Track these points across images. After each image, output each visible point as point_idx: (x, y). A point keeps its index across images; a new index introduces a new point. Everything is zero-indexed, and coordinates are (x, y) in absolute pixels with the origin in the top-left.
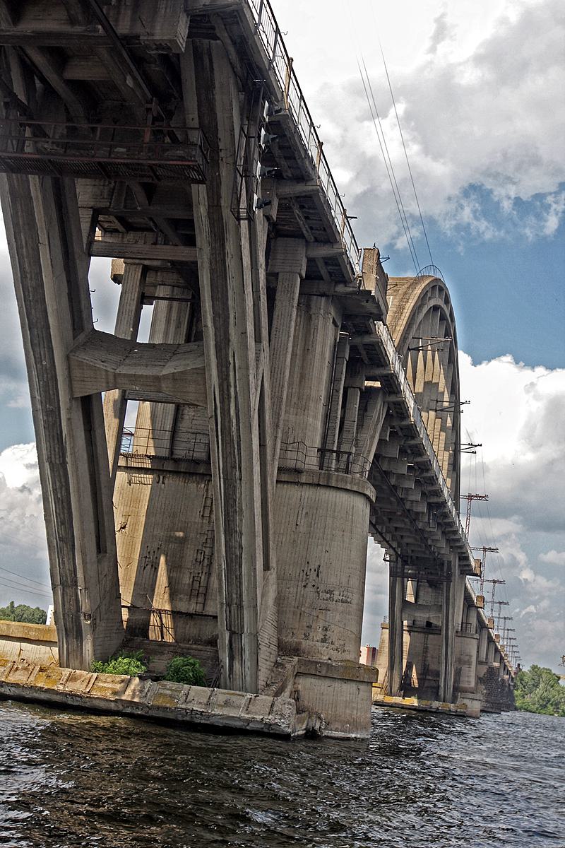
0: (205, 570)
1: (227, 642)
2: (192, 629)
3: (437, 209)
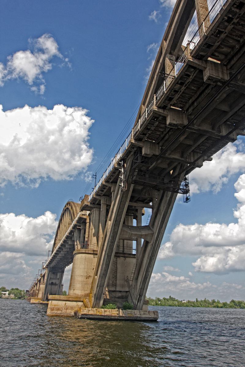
0: (115, 279)
1: (138, 298)
2: (114, 294)
3: (12, 179)
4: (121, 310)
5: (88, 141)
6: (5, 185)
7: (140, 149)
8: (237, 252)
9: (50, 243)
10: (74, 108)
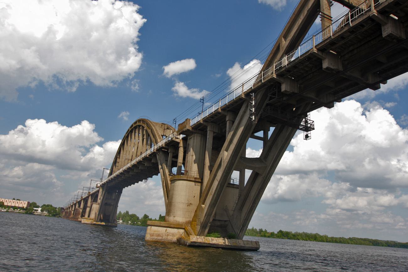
3: (45, 79)
4: (226, 239)
5: (138, 43)
6: (36, 86)
7: (280, 84)
8: (288, 181)
9: (86, 156)
10: (124, 1)
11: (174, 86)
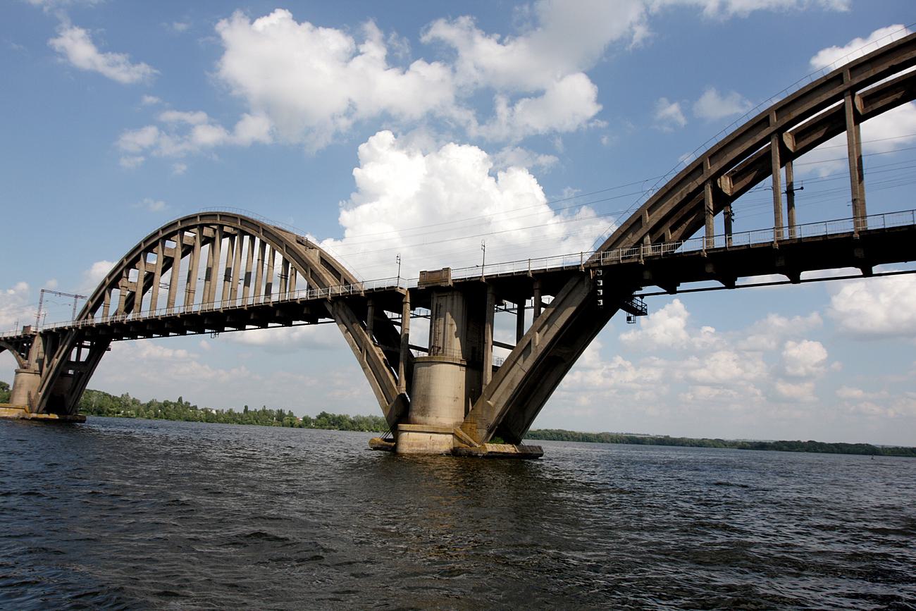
11: (57, 36)
